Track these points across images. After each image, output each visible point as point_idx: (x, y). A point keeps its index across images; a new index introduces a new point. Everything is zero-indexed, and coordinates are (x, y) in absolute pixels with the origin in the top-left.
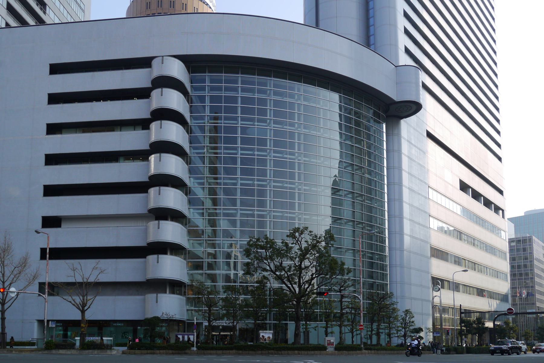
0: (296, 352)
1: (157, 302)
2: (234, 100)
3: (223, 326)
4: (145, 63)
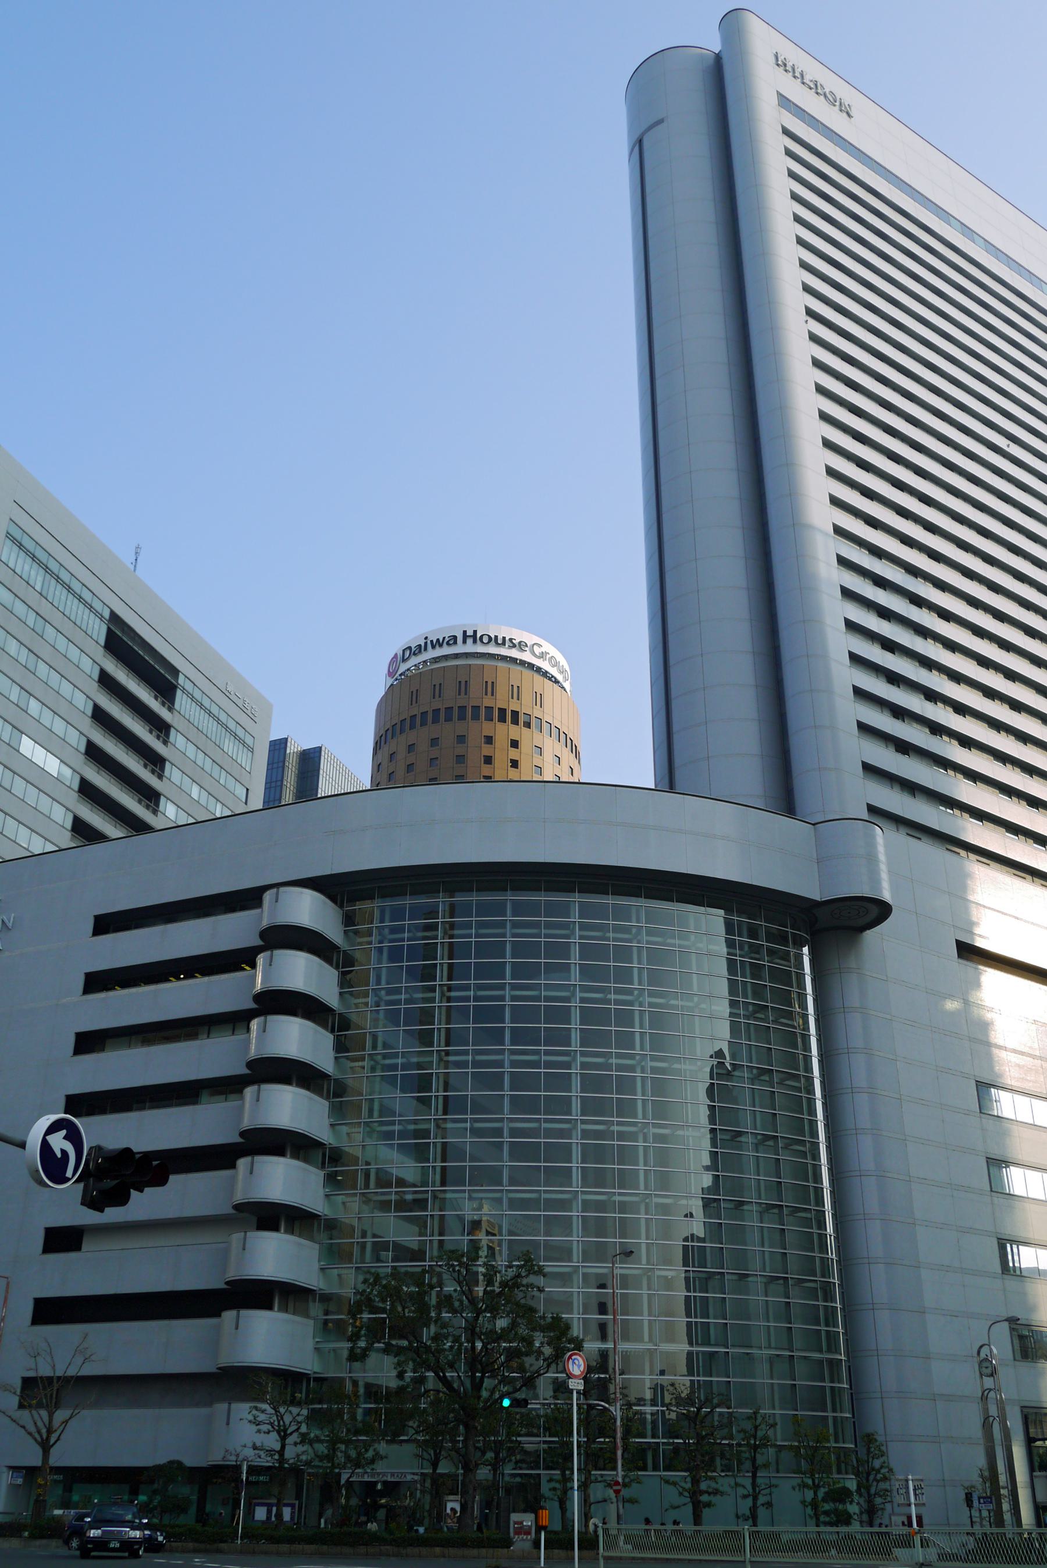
0: (438, 1550)
1: (228, 1424)
2: (498, 949)
3: (385, 1483)
4: (247, 899)
